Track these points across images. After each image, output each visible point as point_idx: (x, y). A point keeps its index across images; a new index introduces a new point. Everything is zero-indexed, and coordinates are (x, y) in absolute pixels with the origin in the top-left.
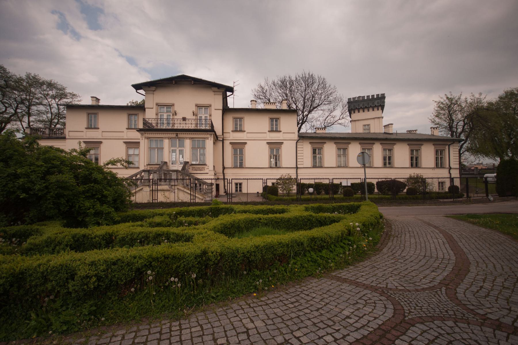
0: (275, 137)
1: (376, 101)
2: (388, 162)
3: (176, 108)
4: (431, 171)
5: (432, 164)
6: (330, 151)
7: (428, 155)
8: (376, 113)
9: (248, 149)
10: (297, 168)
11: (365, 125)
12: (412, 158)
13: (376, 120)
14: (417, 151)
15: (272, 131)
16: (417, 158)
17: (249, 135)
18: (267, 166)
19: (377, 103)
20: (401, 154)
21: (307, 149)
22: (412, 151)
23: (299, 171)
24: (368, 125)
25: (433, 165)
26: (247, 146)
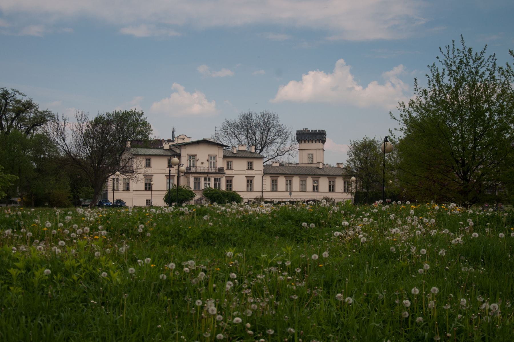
0: (250, 173)
1: (318, 136)
2: (316, 189)
3: (198, 157)
4: (340, 194)
5: (327, 189)
6: (296, 182)
7: (339, 184)
8: (319, 145)
9: (154, 179)
10: (262, 192)
11: (309, 154)
12: (330, 186)
13: (318, 151)
14: (333, 182)
15: (248, 169)
16: (333, 187)
17: (236, 172)
18: (245, 190)
19: (319, 137)
20: (324, 184)
21: (268, 180)
22: (330, 182)
23: (264, 193)
24: (312, 154)
25: (342, 191)
26: (153, 177)
